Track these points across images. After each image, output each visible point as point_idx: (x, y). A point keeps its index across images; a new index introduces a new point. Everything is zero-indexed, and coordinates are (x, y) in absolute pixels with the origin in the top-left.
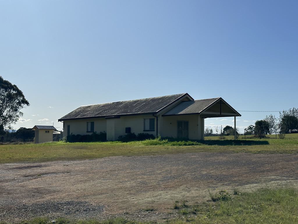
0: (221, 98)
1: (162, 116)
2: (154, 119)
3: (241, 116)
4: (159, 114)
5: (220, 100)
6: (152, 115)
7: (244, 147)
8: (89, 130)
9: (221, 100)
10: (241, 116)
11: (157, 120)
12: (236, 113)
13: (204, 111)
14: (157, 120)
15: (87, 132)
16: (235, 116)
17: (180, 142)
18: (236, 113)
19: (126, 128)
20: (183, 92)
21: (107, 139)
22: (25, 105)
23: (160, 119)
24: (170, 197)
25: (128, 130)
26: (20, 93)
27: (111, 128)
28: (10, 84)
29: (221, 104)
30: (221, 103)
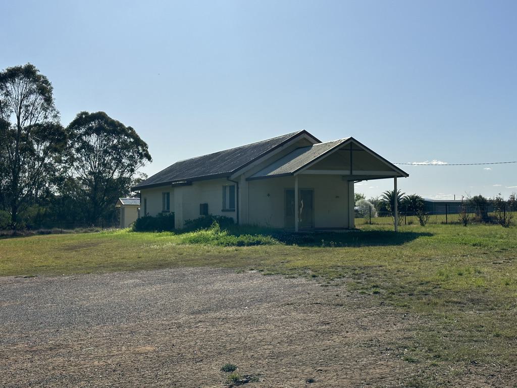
0: (352, 138)
1: (247, 180)
2: (234, 186)
3: (408, 175)
4: (240, 176)
5: (349, 142)
6: (226, 178)
7: (328, 252)
8: (228, 207)
9: (351, 143)
10: (408, 175)
11: (238, 186)
12: (394, 171)
13: (305, 168)
14: (238, 188)
15: (223, 211)
16: (395, 177)
17: (242, 238)
18: (394, 171)
19: (201, 205)
20: (298, 130)
21: (176, 227)
22: (145, 160)
23: (243, 184)
24: (396, 350)
25: (204, 208)
26: (138, 142)
27: (182, 203)
28: (121, 125)
29: (353, 152)
30: (353, 148)
